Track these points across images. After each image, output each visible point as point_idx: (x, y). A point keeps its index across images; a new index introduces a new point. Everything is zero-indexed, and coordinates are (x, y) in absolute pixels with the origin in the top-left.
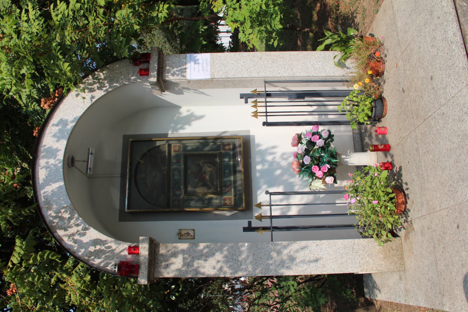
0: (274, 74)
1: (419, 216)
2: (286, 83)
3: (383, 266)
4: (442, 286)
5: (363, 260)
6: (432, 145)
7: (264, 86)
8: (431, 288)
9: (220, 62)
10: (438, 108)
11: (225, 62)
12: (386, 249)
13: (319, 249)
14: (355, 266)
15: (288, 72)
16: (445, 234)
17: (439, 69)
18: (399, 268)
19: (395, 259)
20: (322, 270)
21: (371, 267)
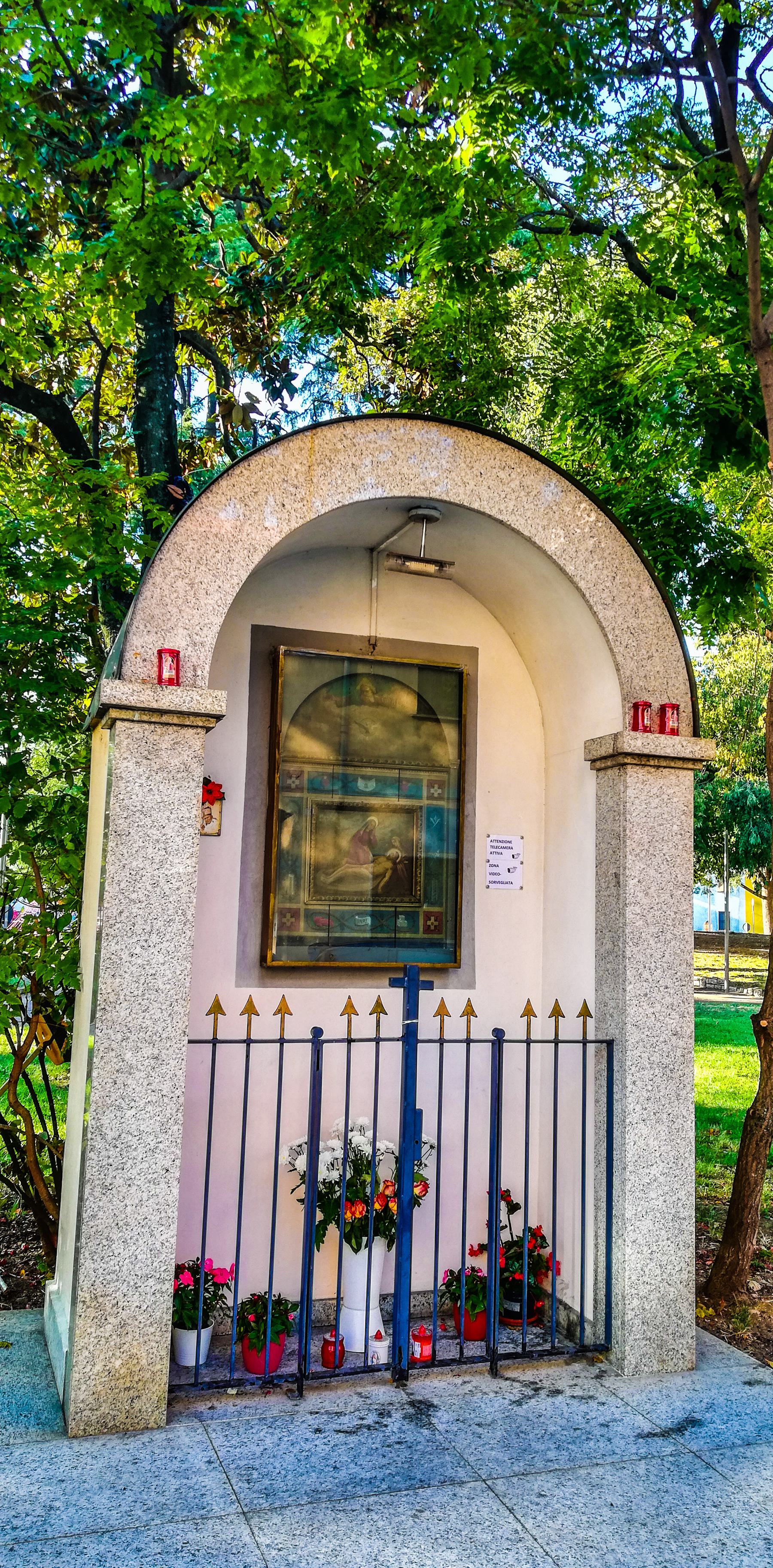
0: (633, 1068)
1: (233, 1481)
2: (605, 1100)
3: (89, 1367)
4: (40, 1548)
5: (113, 1306)
6: (443, 1528)
7: (600, 1038)
8: (27, 1515)
9: (670, 922)
10: (548, 1550)
11: (669, 936)
12: (136, 1379)
13: (155, 1175)
14: (97, 1282)
15: (638, 1108)
16: (191, 1557)
17: (660, 1559)
18: (78, 1417)
19: (105, 1409)
20: (97, 1182)
21: (89, 1330)
